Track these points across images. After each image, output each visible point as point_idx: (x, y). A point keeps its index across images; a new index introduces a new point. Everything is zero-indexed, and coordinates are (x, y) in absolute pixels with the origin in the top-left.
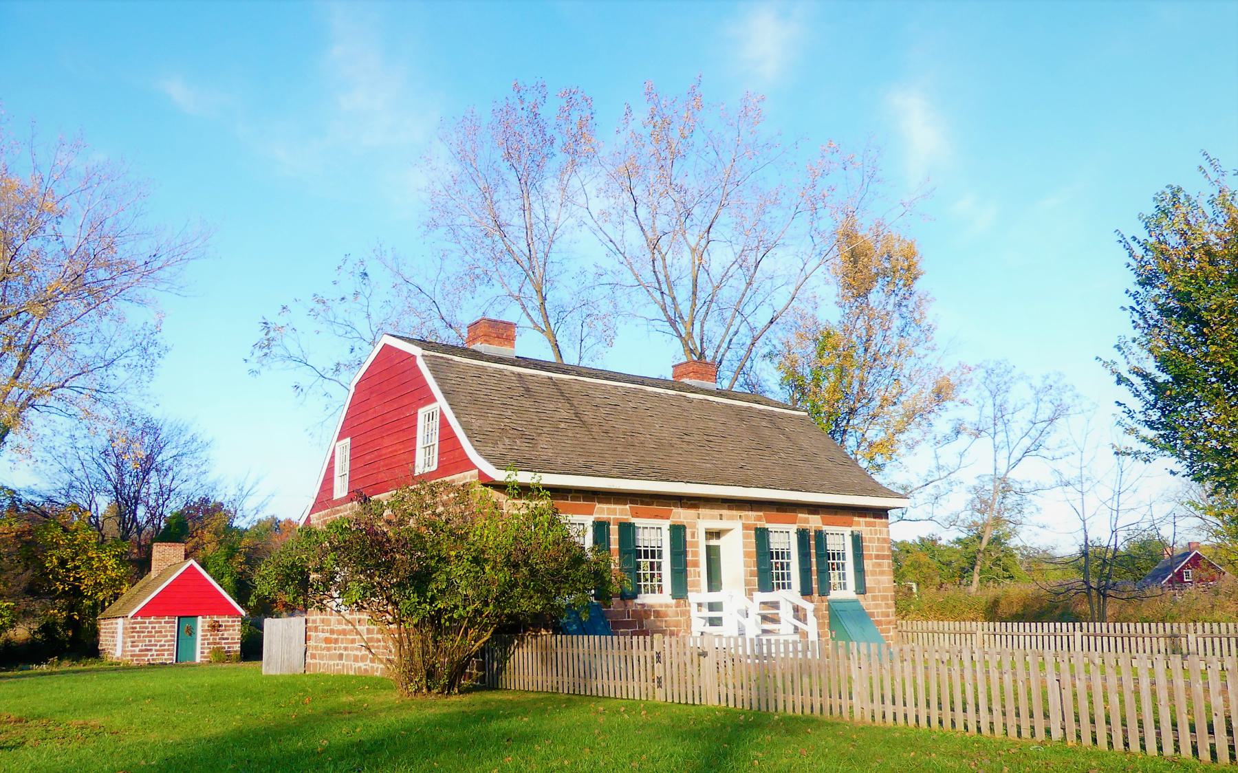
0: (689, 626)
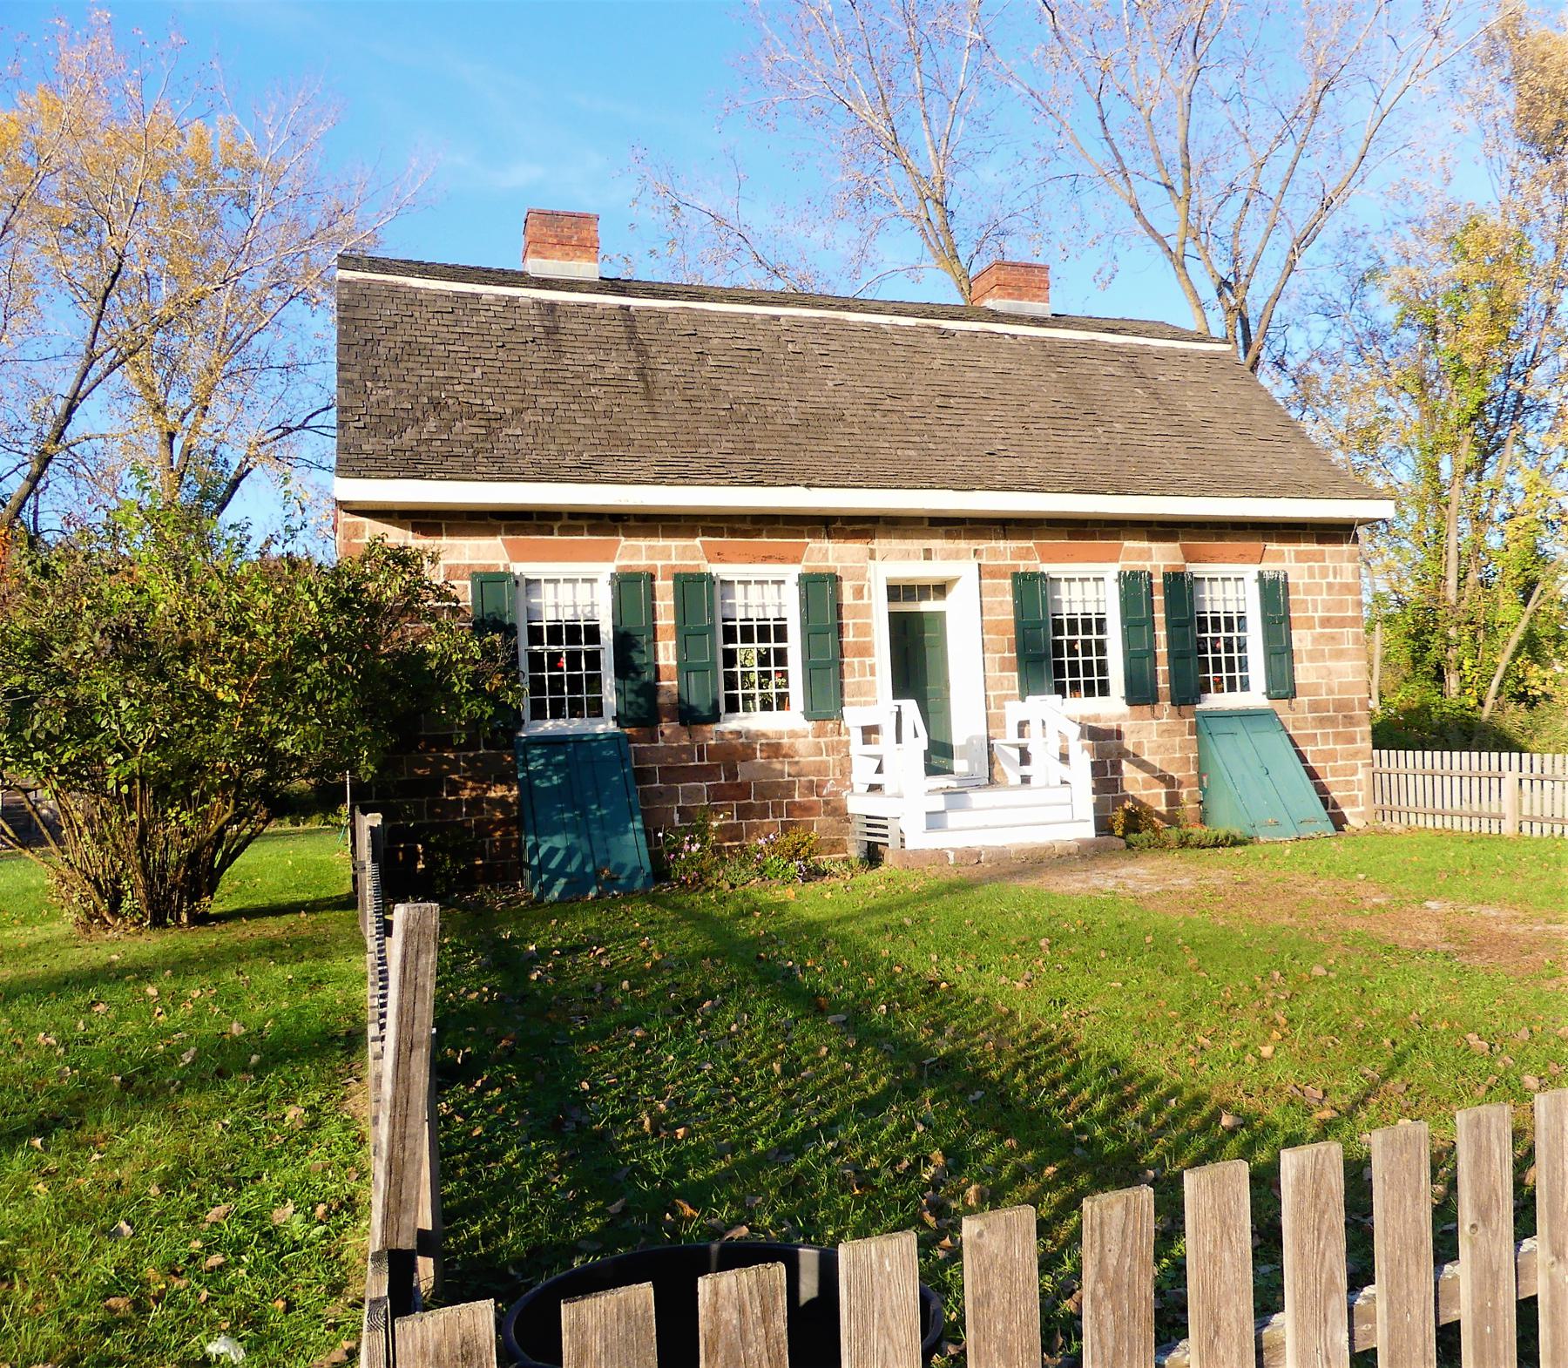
0: (846, 772)
